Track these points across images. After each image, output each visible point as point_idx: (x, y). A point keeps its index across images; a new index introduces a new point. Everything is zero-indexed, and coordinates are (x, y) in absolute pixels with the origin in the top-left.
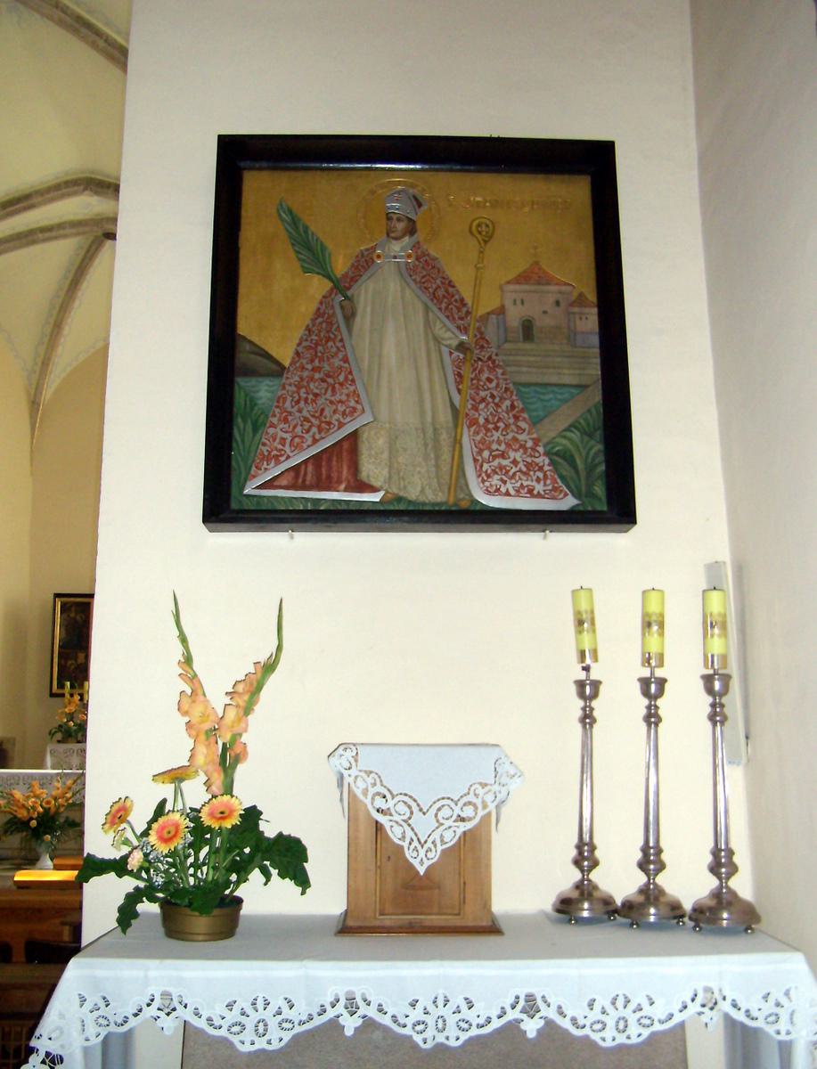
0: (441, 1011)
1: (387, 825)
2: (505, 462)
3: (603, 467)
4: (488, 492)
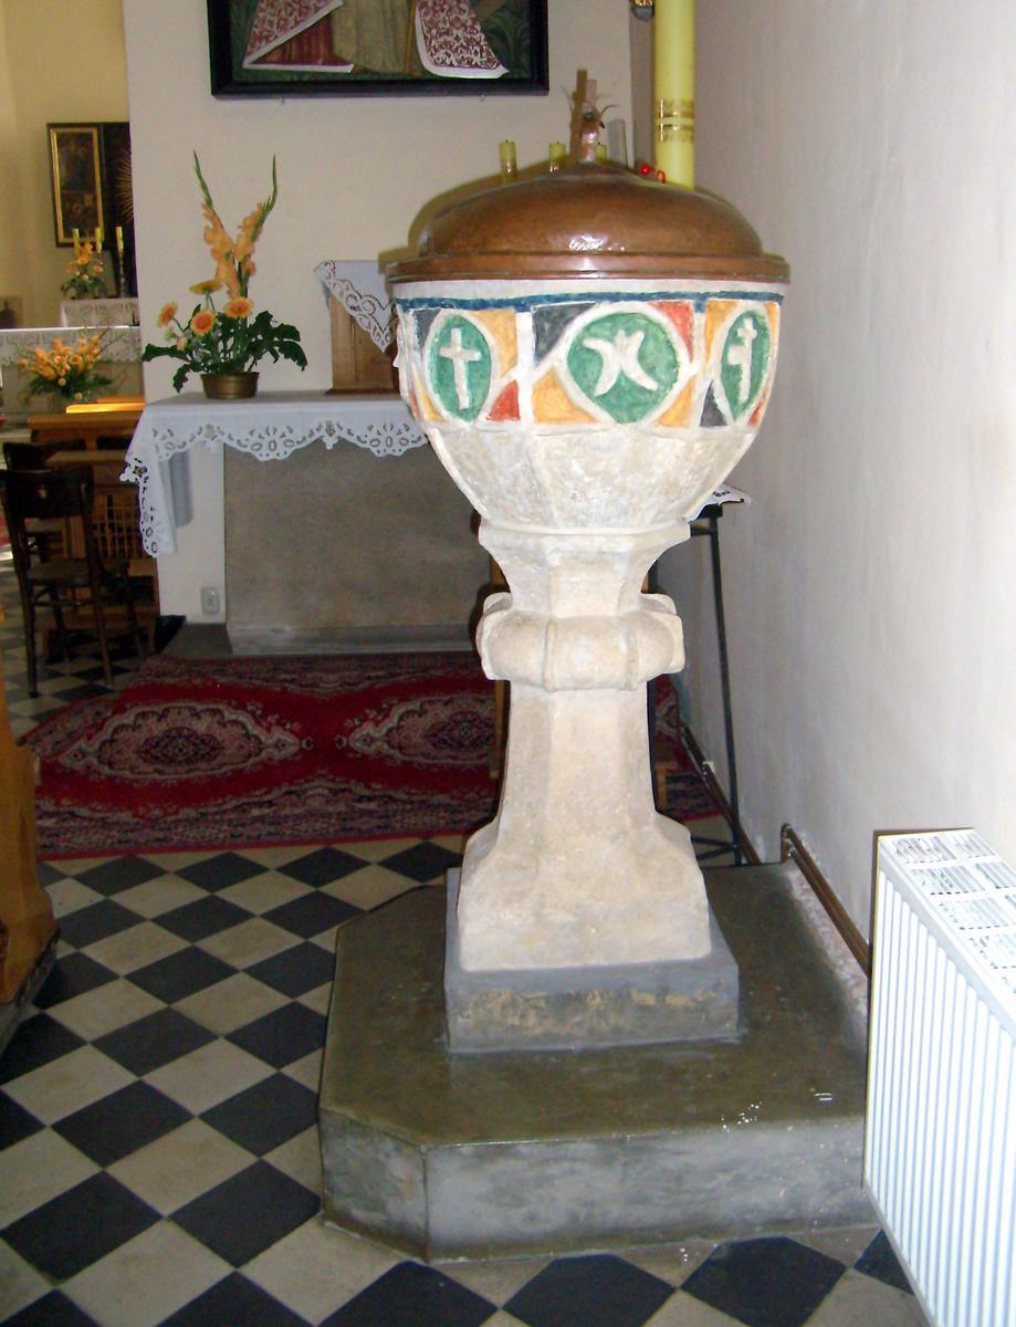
0: (390, 434)
1: (357, 318)
2: (449, 39)
3: (528, 42)
4: (436, 64)
